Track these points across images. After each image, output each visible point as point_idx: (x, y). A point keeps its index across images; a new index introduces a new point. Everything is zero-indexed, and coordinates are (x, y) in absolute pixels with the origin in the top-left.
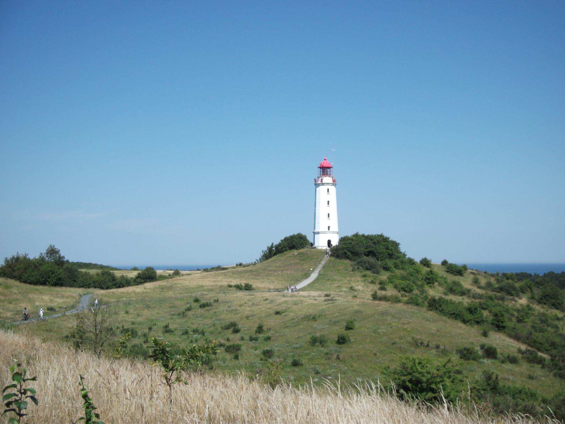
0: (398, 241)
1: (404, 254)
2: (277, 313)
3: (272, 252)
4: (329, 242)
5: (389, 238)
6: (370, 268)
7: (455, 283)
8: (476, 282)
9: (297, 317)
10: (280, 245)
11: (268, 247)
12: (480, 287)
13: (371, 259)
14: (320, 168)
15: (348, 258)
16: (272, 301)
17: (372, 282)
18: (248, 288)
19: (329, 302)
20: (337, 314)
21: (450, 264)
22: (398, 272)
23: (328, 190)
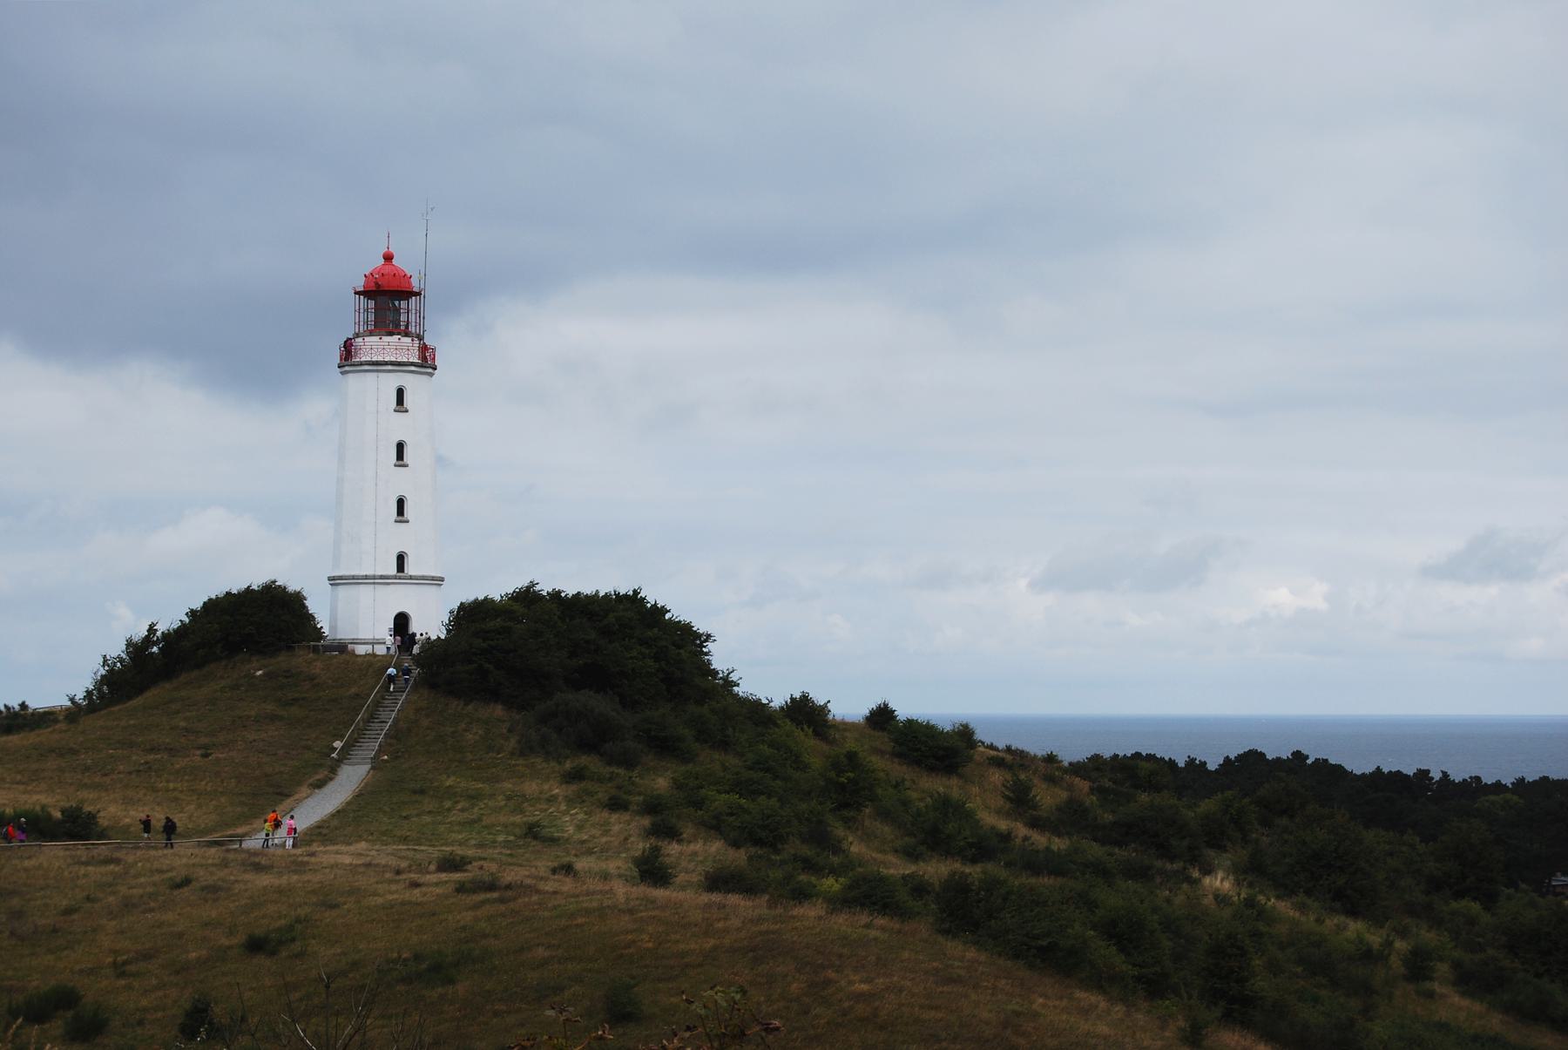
0: (700, 626)
1: (726, 679)
2: (256, 945)
3: (144, 669)
4: (401, 621)
5: (664, 611)
6: (595, 738)
7: (946, 806)
8: (1019, 800)
9: (355, 965)
10: (182, 632)
11: (129, 643)
12: (1034, 824)
13: (600, 704)
14: (366, 293)
15: (493, 695)
16: (213, 889)
17: (616, 805)
18: (78, 826)
19: (482, 896)
20: (541, 952)
21: (911, 723)
22: (712, 761)
23: (400, 393)
